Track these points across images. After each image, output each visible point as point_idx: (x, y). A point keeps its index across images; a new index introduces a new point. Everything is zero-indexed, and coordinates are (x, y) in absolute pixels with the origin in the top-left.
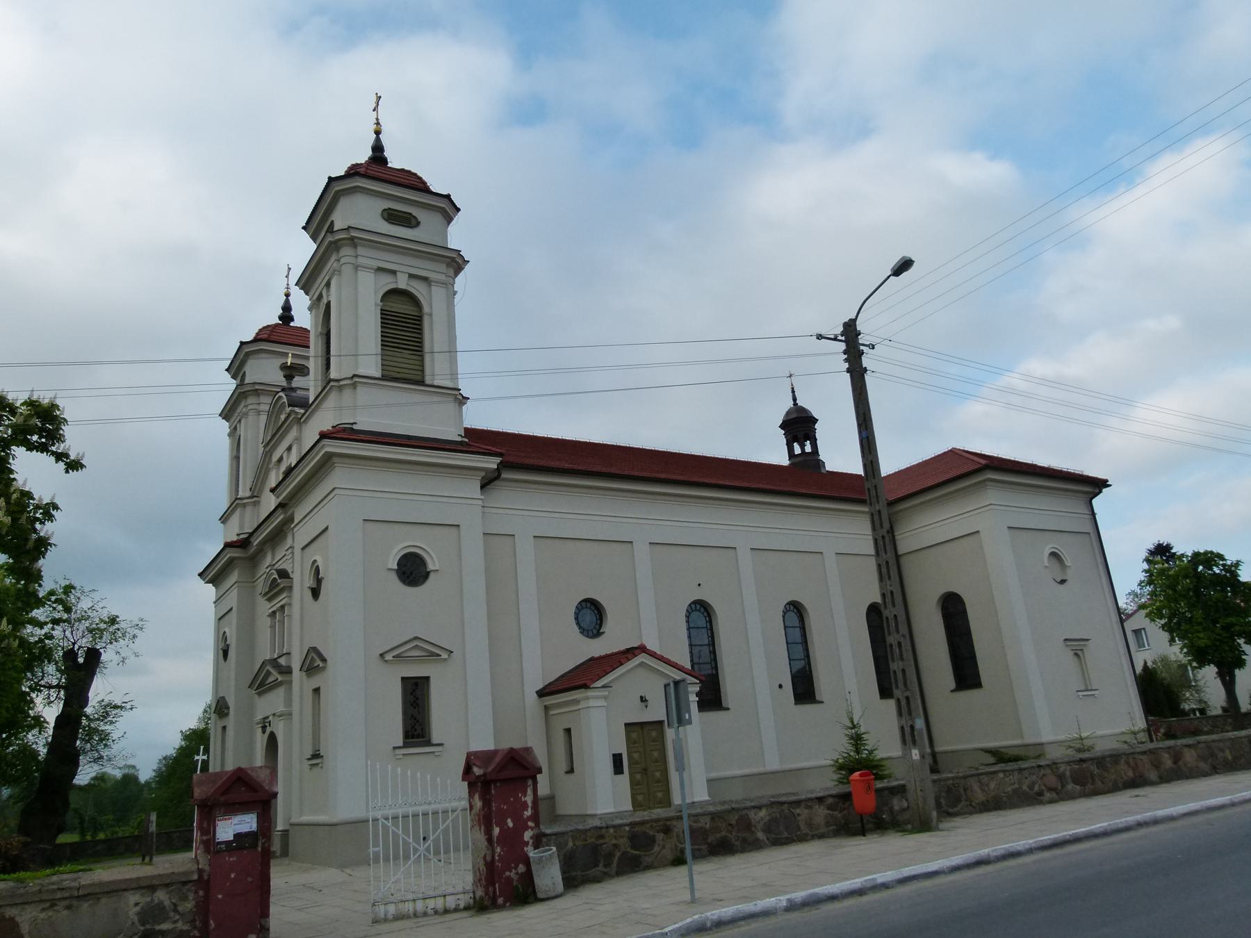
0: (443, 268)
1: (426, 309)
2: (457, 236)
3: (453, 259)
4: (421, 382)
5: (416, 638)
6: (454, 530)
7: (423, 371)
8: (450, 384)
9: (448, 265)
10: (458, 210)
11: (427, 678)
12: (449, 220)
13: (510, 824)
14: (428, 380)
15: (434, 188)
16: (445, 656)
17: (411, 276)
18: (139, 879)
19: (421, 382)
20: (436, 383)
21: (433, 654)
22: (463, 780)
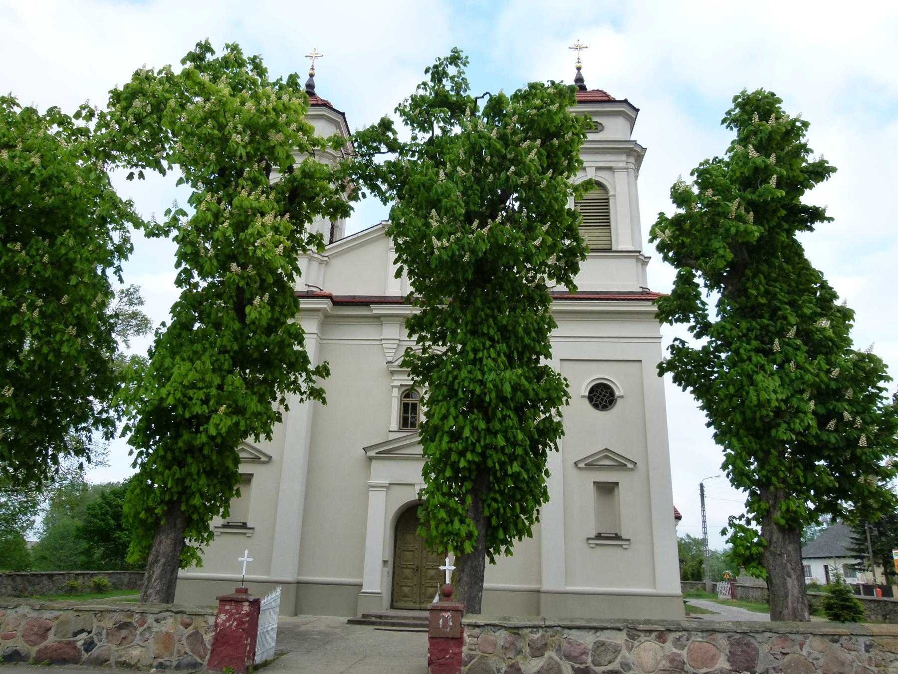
0: (624, 158)
1: (611, 193)
2: (640, 134)
3: (631, 150)
4: (610, 250)
5: (607, 450)
6: (638, 364)
7: (610, 236)
8: (633, 249)
9: (628, 155)
10: (638, 110)
11: (617, 484)
12: (632, 122)
13: (822, 462)
14: (613, 249)
15: (624, 537)
16: (630, 466)
17: (598, 169)
18: (740, 606)
19: (610, 250)
20: (619, 249)
21: (622, 465)
22: (717, 306)
